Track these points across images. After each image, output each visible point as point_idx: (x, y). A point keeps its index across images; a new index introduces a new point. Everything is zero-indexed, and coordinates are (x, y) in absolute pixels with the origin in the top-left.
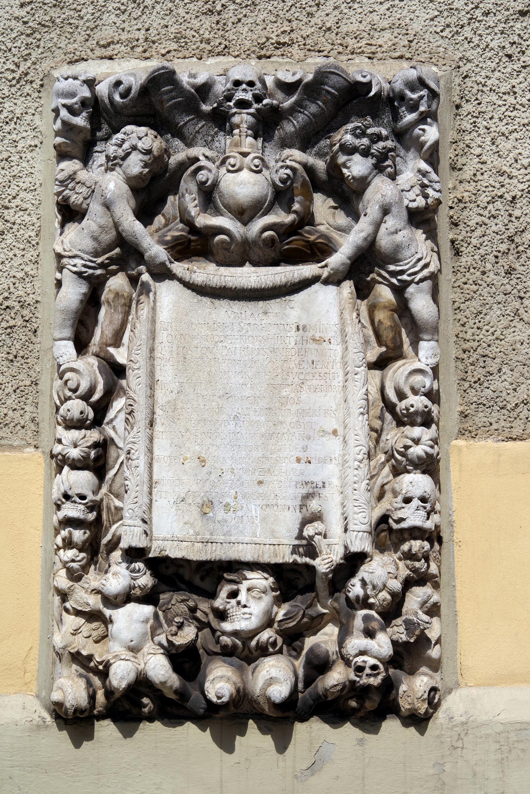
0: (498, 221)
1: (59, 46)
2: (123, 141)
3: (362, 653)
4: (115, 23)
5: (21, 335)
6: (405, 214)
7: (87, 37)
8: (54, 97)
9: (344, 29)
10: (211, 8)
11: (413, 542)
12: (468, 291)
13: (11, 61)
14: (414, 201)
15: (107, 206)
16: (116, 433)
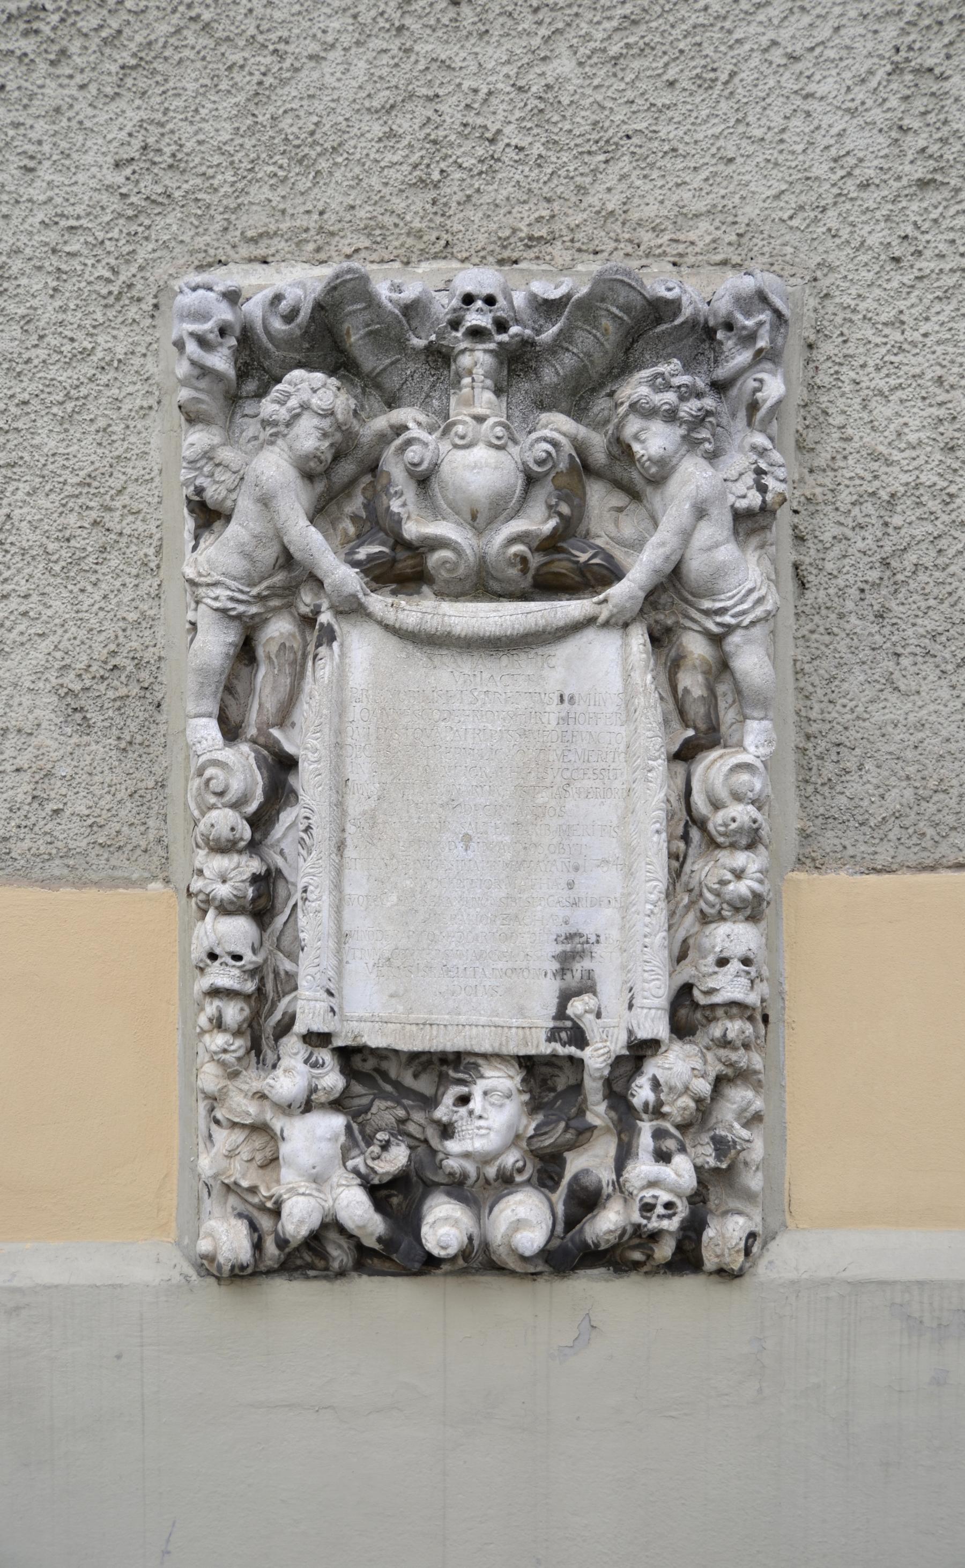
0: (867, 534)
1: (180, 238)
2: (288, 395)
3: (652, 1184)
4: (270, 201)
5: (137, 710)
6: (728, 517)
7: (225, 224)
8: (176, 321)
9: (635, 215)
10: (424, 177)
11: (729, 1025)
12: (815, 645)
13: (104, 263)
14: (744, 497)
15: (265, 501)
16: (286, 859)
